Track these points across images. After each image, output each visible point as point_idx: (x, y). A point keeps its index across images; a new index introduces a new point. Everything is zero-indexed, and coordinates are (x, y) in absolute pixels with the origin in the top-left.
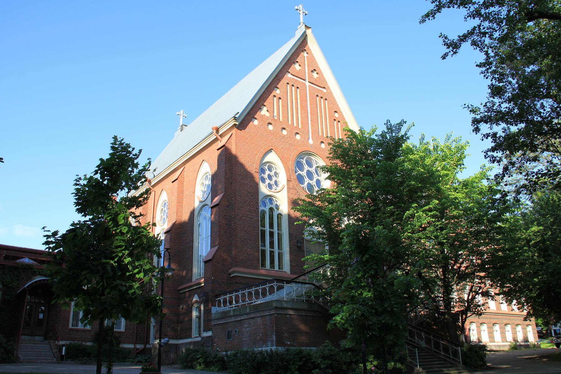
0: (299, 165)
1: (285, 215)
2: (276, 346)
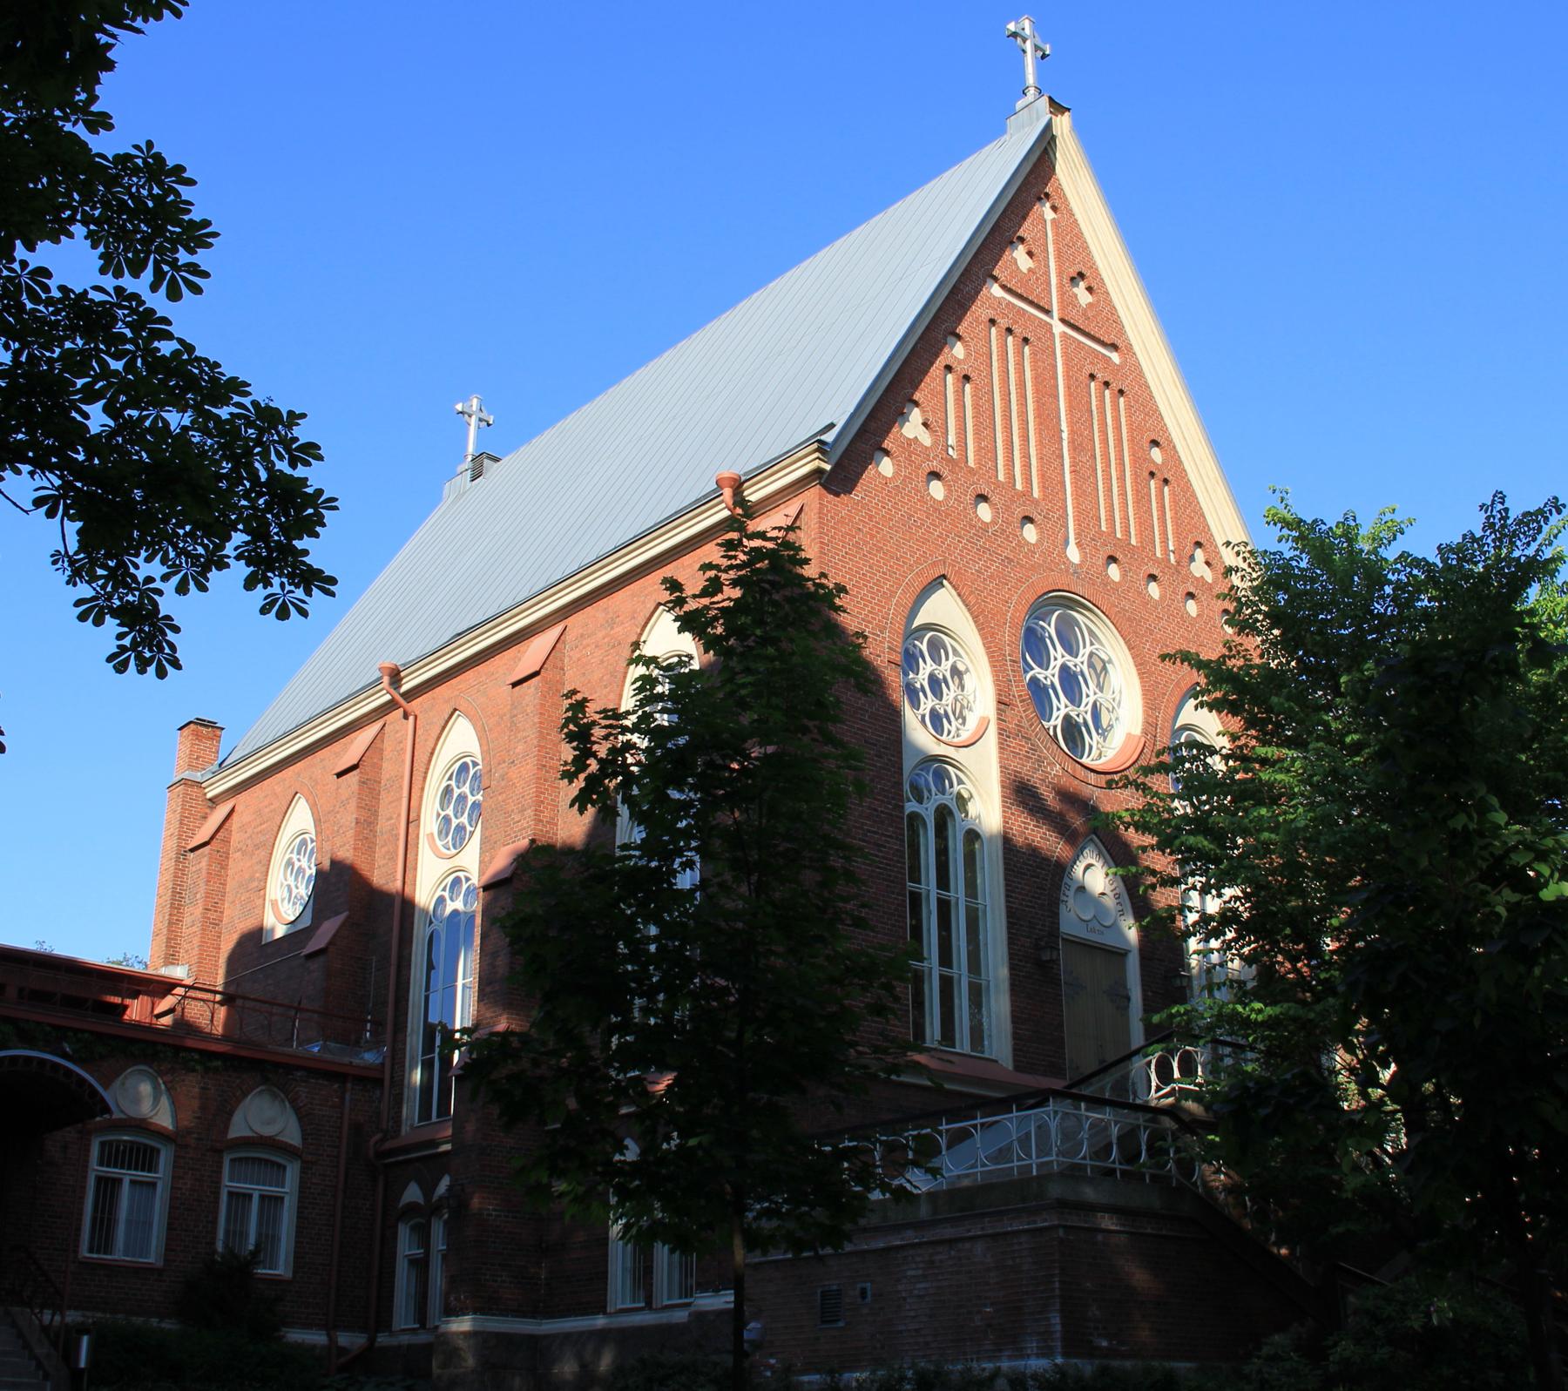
0: (1034, 645)
1: (991, 838)
2: (1065, 1355)
